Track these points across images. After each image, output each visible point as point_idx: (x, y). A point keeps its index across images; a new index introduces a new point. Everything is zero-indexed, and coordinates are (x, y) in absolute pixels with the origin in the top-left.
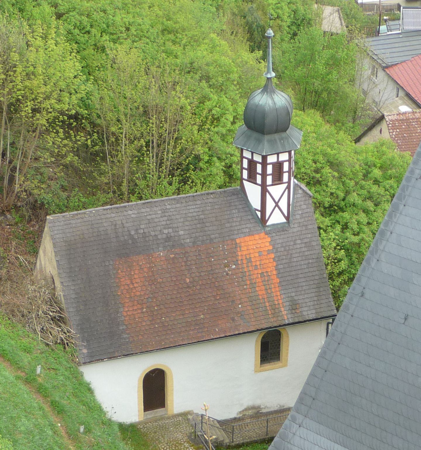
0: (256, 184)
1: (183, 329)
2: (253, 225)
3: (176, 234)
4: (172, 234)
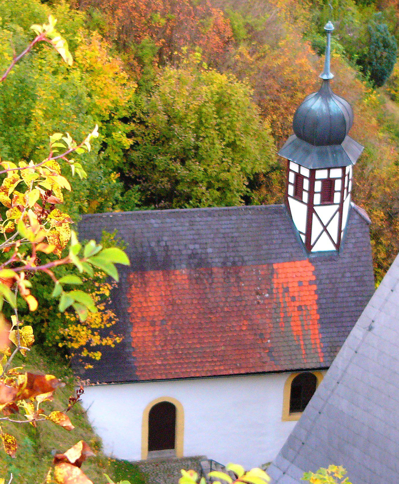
0: (302, 202)
1: (199, 360)
2: (295, 250)
3: (203, 251)
4: (199, 251)
